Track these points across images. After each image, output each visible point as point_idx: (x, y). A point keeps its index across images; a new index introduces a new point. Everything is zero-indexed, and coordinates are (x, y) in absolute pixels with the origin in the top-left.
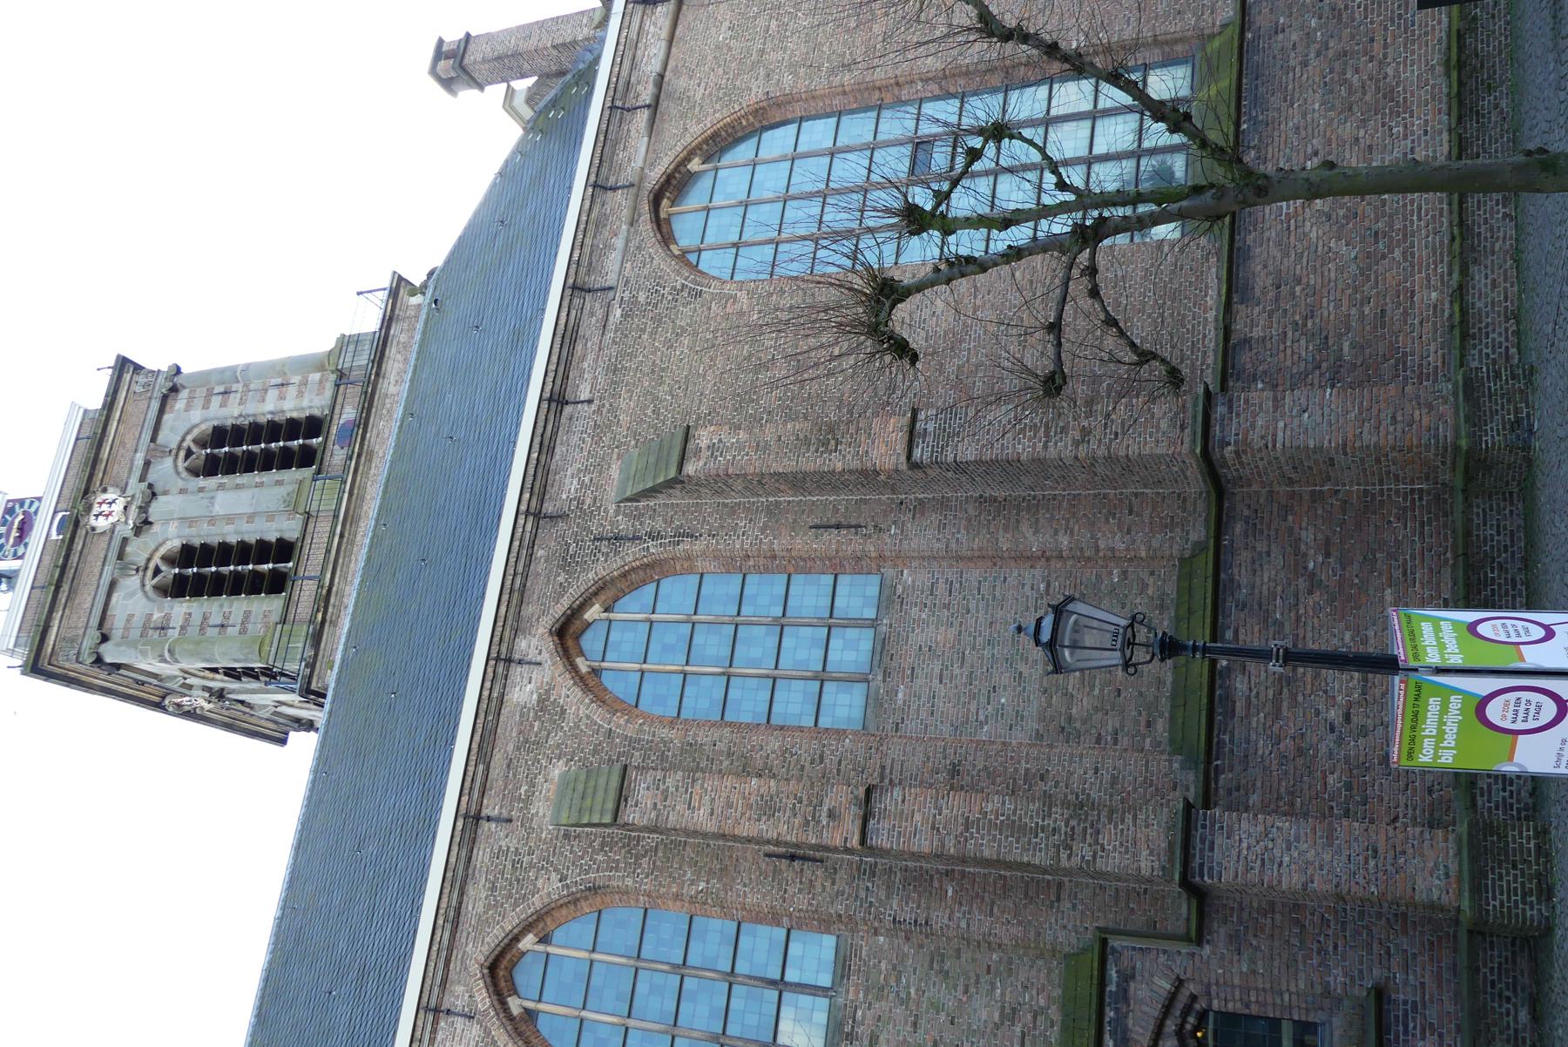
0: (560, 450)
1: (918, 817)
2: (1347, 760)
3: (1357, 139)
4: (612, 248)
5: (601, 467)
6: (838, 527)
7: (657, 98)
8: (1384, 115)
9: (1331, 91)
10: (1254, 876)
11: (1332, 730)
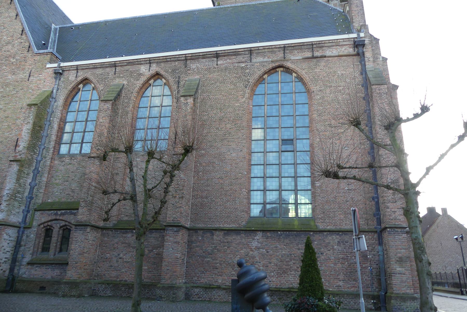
0: (204, 60)
1: (93, 168)
2: (112, 258)
3: (271, 263)
4: (264, 57)
5: (199, 73)
6: (176, 138)
7: (317, 57)
8: (278, 270)
9: (288, 256)
10: (74, 239)
11: (118, 255)
